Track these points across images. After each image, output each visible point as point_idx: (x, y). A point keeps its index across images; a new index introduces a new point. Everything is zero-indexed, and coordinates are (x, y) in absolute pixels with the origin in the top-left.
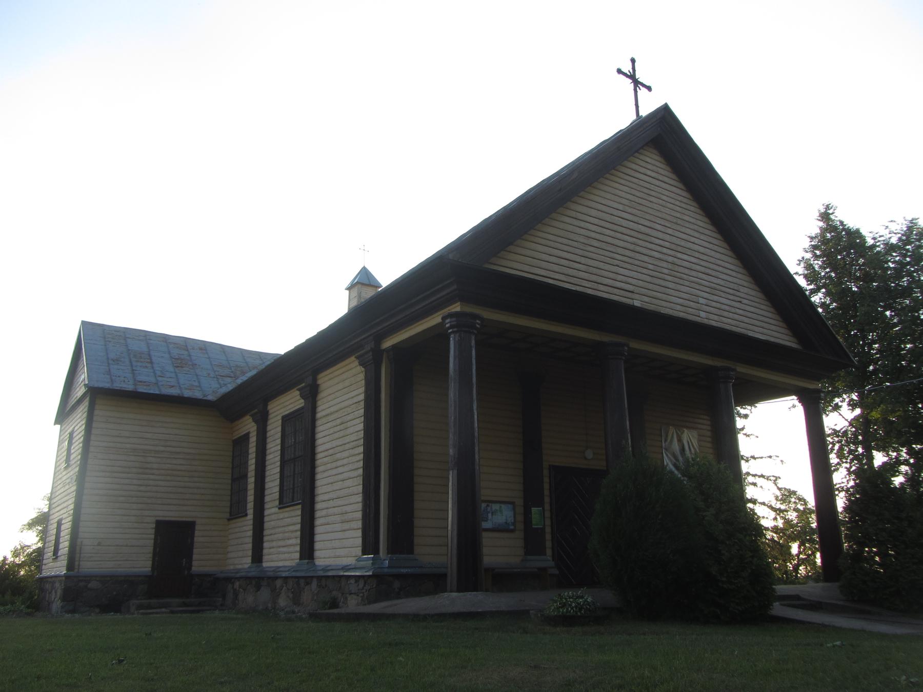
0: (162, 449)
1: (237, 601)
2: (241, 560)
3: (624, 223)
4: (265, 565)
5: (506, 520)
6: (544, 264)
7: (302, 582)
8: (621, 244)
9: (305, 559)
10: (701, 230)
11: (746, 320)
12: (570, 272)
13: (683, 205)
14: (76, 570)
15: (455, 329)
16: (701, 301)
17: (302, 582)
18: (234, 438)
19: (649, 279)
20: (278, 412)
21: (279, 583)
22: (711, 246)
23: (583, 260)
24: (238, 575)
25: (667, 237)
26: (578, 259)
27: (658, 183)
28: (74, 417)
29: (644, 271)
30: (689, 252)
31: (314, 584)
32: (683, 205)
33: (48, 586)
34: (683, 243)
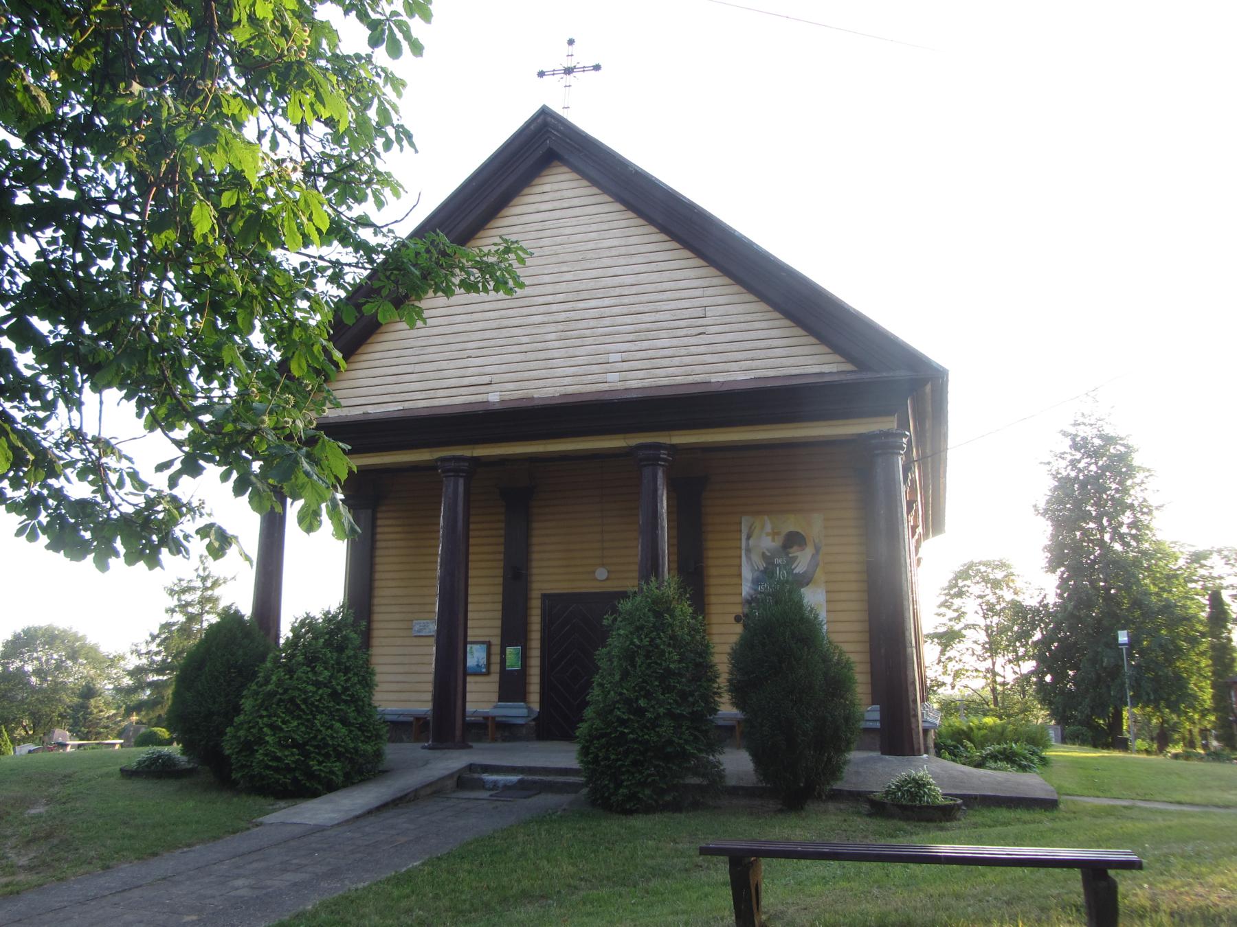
5: (478, 661)
10: (653, 257)
12: (397, 388)
22: (653, 267)
23: (418, 368)
27: (558, 214)
30: (600, 293)
33: (367, 689)
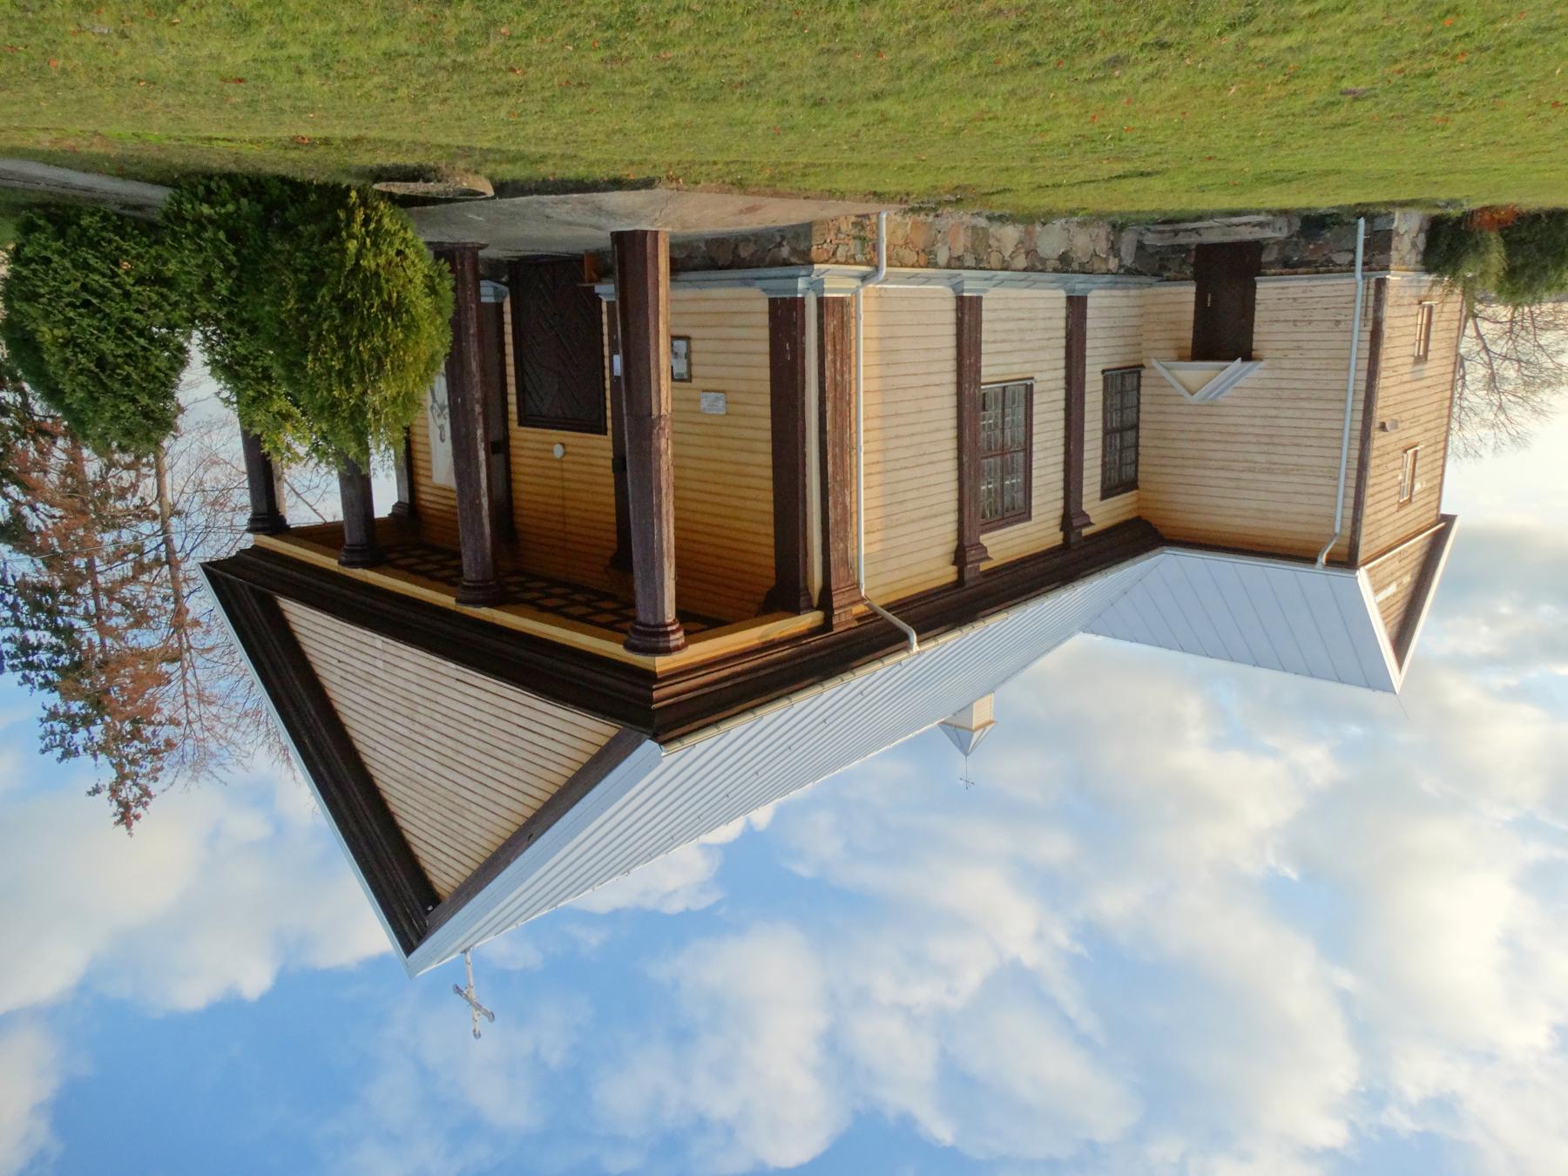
0: (1245, 475)
1: (1112, 238)
2: (1103, 302)
3: (470, 784)
4: (1062, 294)
6: (559, 725)
7: (970, 260)
8: (472, 753)
9: (971, 298)
11: (332, 634)
13: (404, 806)
14: (1373, 280)
15: (661, 630)
16: (380, 664)
17: (970, 260)
18: (1135, 492)
19: (439, 698)
20: (1038, 528)
21: (1021, 261)
24: (1108, 278)
25: (421, 760)
26: (519, 732)
27: (434, 842)
28: (1402, 529)
29: (444, 711)
31: (942, 257)
32: (404, 806)
34: (404, 751)
